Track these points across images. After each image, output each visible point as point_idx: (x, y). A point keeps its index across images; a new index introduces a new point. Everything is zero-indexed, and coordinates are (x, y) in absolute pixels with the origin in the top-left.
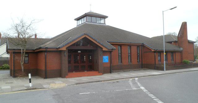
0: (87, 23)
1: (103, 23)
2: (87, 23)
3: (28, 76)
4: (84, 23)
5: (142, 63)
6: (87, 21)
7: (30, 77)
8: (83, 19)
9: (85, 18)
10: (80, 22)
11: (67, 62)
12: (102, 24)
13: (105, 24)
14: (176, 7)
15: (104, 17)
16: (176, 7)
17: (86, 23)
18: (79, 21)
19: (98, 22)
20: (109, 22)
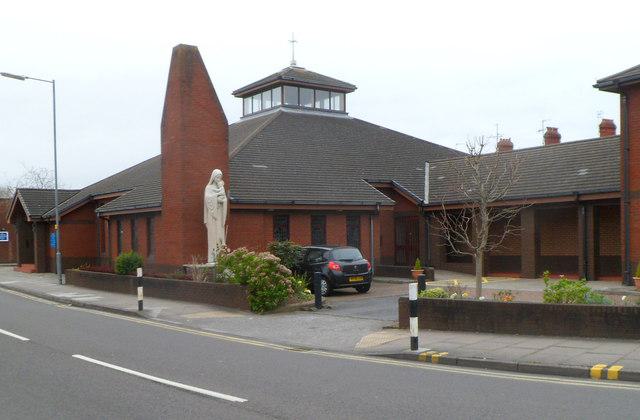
0: (284, 110)
1: (338, 109)
2: (284, 110)
3: (136, 293)
4: (272, 108)
5: (133, 231)
6: (283, 106)
7: (140, 297)
8: (267, 94)
9: (277, 91)
10: (255, 104)
11: (523, 263)
12: (335, 112)
13: (344, 112)
14: (4, 74)
15: (344, 89)
16: (4, 74)
17: (283, 113)
18: (249, 99)
19: (310, 106)
20: (357, 108)
